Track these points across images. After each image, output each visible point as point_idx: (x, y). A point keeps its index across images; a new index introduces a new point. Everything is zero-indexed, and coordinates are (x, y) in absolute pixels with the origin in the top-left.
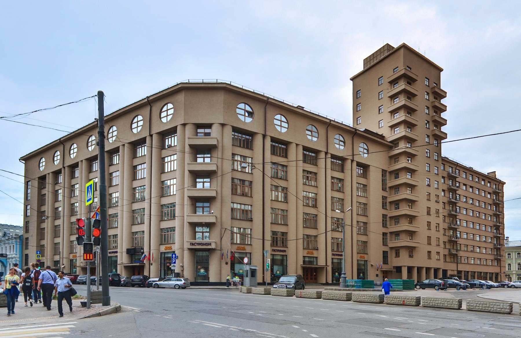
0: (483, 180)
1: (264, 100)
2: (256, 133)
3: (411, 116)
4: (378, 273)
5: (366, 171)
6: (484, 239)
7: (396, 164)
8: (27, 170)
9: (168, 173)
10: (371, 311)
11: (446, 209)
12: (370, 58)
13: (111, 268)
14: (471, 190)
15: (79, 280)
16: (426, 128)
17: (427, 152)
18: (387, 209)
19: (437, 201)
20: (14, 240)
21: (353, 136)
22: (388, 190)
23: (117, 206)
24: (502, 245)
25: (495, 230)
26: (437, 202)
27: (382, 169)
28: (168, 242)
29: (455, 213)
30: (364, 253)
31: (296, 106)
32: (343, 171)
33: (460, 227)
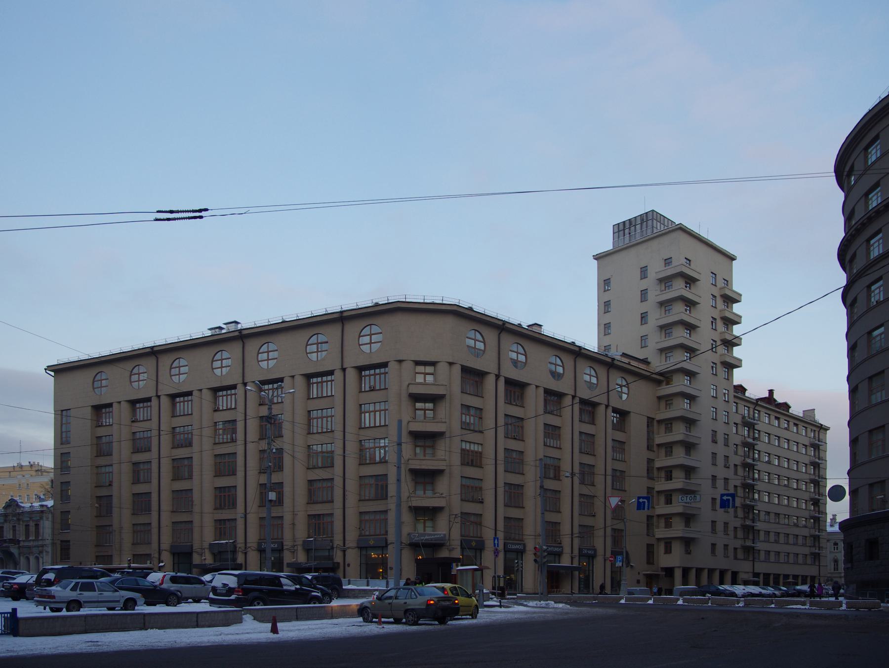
0: (796, 425)
1: (869, 148)
2: (487, 373)
5: (624, 420)
8: (855, 454)
9: (380, 428)
11: (739, 474)
12: (647, 216)
13: (872, 262)
14: (776, 423)
15: (884, 607)
17: (725, 394)
18: (654, 451)
21: (500, 334)
22: (655, 448)
23: (149, 420)
24: (822, 512)
27: (648, 417)
28: (508, 595)
29: (751, 482)
30: (476, 394)
32: (593, 422)
33: (758, 463)
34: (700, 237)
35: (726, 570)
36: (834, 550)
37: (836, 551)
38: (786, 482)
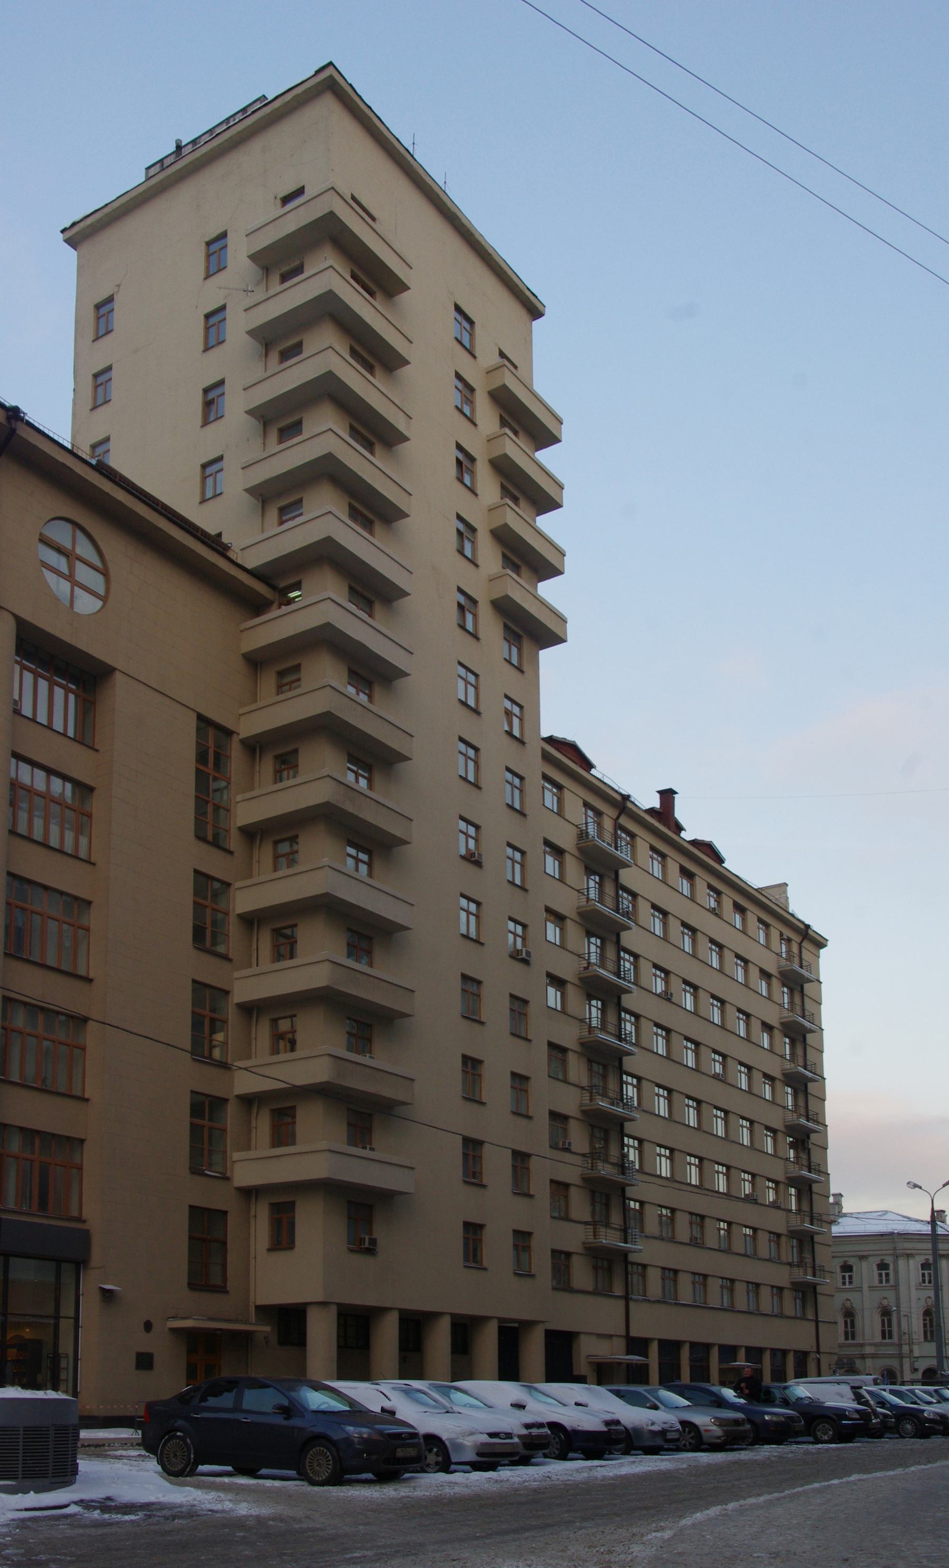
3: (370, 698)
4: (144, 1343)
6: (747, 1188)
7: (280, 874)
10: (98, 1457)
16: (505, 737)
19: (519, 952)
20: (626, 976)
22: (235, 842)
25: (791, 1148)
26: (521, 1114)
27: (201, 718)
31: (756, 888)
34: (412, 161)
35: (527, 1325)
36: (844, 1283)
37: (847, 1286)
38: (718, 1069)
